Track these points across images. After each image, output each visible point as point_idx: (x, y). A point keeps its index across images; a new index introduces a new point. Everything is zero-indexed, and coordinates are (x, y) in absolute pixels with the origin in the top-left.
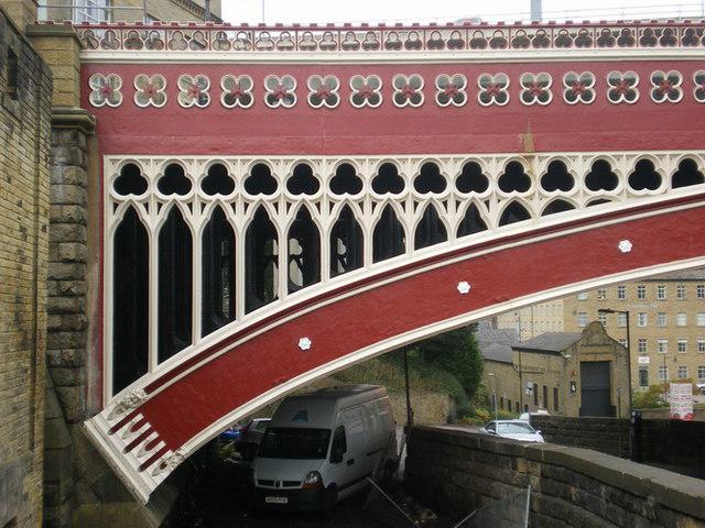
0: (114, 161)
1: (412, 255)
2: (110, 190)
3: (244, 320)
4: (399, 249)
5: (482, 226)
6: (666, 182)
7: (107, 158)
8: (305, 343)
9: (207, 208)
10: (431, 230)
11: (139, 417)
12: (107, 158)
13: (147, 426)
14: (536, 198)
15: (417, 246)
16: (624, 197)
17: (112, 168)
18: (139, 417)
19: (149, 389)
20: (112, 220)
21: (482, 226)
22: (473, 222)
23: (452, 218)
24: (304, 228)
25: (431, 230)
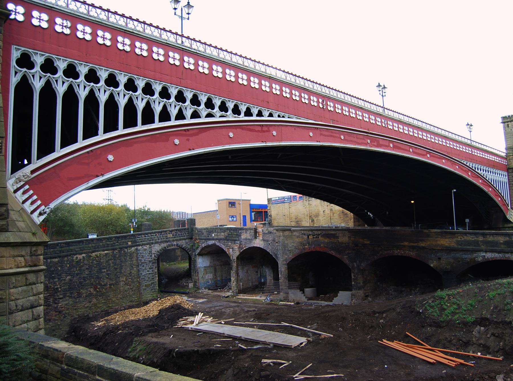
0: (17, 49)
1: (157, 124)
2: (14, 63)
3: (81, 143)
4: (115, 128)
5: (251, 115)
6: (243, 114)
7: (14, 47)
8: (111, 158)
9: (42, 80)
10: (165, 116)
11: (27, 187)
12: (14, 47)
13: (31, 192)
14: (203, 110)
15: (84, 139)
16: (230, 116)
17: (16, 54)
18: (27, 187)
19: (33, 172)
20: (14, 80)
21: (239, 113)
22: (180, 116)
23: (174, 112)
24: (130, 106)
25: (165, 116)
